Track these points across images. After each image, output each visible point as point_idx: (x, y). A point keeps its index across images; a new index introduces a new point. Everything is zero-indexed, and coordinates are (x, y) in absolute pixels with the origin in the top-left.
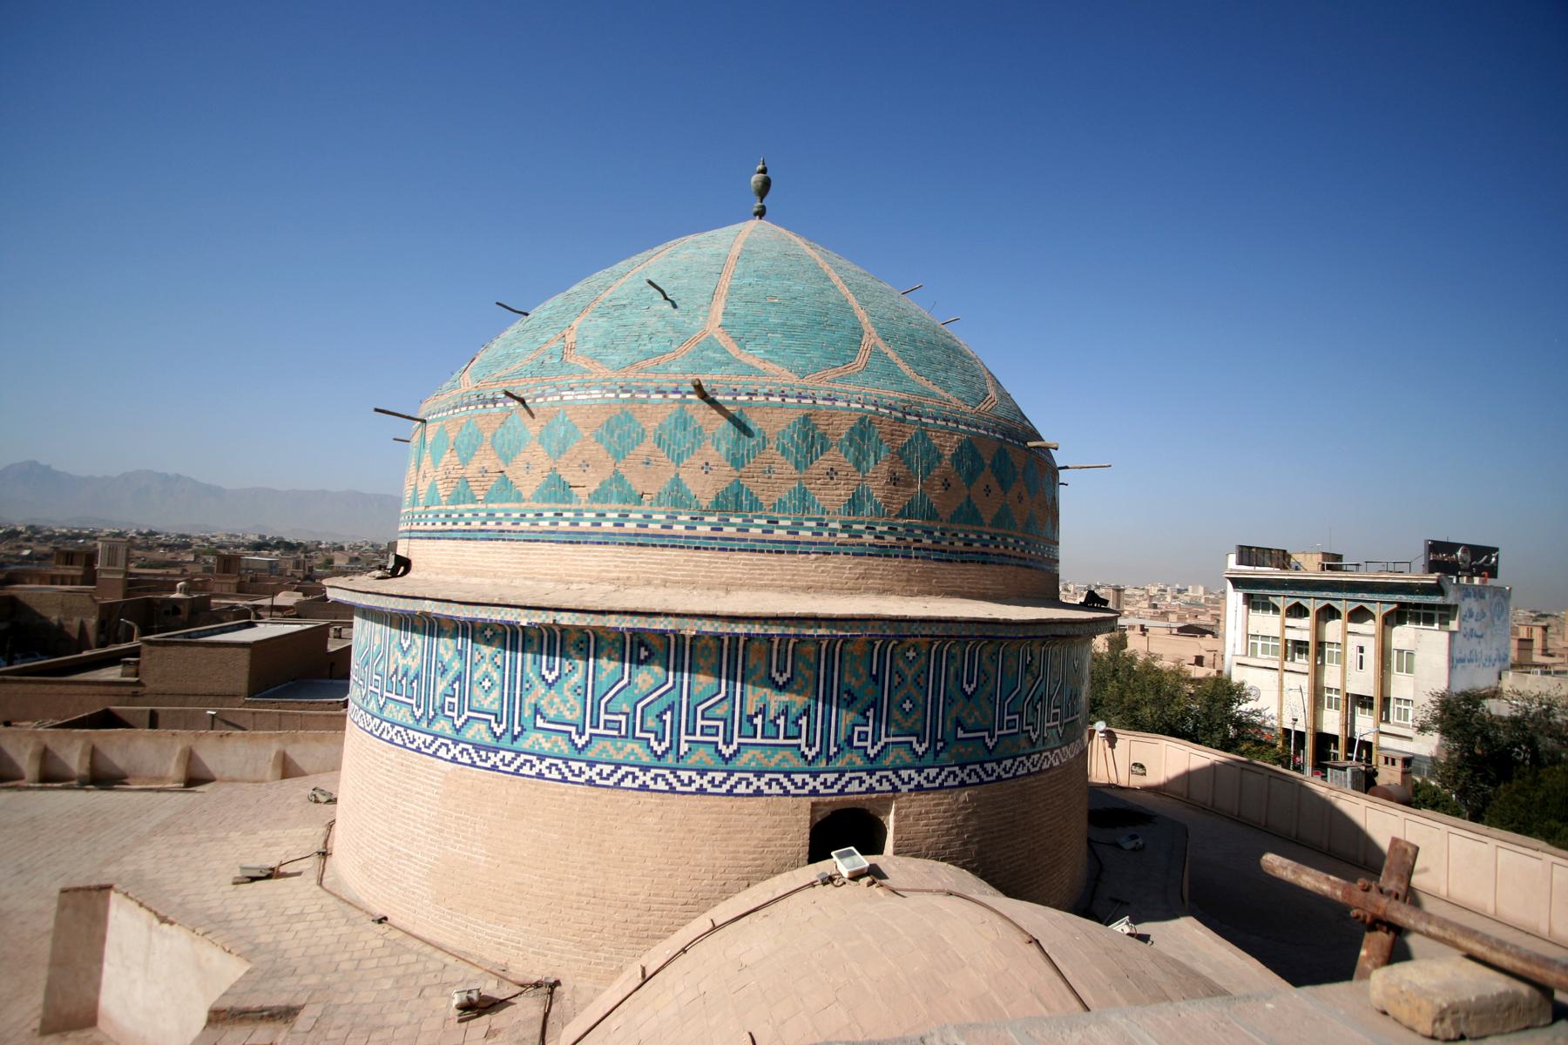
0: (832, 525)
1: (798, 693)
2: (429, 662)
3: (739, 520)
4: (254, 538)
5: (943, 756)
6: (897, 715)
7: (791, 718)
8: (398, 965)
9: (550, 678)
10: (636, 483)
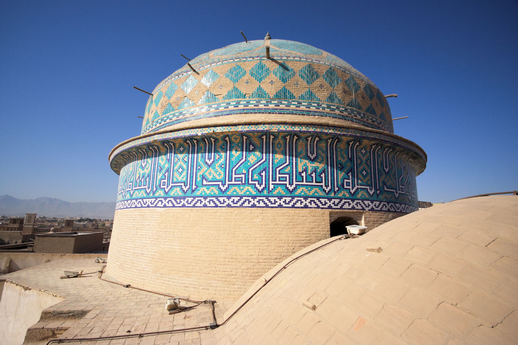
0: (323, 106)
1: (320, 163)
2: (154, 168)
3: (286, 102)
4: (79, 218)
5: (380, 196)
6: (360, 176)
7: (318, 174)
8: (136, 298)
9: (209, 163)
10: (243, 90)
